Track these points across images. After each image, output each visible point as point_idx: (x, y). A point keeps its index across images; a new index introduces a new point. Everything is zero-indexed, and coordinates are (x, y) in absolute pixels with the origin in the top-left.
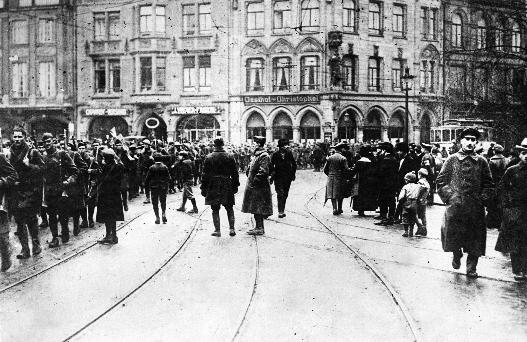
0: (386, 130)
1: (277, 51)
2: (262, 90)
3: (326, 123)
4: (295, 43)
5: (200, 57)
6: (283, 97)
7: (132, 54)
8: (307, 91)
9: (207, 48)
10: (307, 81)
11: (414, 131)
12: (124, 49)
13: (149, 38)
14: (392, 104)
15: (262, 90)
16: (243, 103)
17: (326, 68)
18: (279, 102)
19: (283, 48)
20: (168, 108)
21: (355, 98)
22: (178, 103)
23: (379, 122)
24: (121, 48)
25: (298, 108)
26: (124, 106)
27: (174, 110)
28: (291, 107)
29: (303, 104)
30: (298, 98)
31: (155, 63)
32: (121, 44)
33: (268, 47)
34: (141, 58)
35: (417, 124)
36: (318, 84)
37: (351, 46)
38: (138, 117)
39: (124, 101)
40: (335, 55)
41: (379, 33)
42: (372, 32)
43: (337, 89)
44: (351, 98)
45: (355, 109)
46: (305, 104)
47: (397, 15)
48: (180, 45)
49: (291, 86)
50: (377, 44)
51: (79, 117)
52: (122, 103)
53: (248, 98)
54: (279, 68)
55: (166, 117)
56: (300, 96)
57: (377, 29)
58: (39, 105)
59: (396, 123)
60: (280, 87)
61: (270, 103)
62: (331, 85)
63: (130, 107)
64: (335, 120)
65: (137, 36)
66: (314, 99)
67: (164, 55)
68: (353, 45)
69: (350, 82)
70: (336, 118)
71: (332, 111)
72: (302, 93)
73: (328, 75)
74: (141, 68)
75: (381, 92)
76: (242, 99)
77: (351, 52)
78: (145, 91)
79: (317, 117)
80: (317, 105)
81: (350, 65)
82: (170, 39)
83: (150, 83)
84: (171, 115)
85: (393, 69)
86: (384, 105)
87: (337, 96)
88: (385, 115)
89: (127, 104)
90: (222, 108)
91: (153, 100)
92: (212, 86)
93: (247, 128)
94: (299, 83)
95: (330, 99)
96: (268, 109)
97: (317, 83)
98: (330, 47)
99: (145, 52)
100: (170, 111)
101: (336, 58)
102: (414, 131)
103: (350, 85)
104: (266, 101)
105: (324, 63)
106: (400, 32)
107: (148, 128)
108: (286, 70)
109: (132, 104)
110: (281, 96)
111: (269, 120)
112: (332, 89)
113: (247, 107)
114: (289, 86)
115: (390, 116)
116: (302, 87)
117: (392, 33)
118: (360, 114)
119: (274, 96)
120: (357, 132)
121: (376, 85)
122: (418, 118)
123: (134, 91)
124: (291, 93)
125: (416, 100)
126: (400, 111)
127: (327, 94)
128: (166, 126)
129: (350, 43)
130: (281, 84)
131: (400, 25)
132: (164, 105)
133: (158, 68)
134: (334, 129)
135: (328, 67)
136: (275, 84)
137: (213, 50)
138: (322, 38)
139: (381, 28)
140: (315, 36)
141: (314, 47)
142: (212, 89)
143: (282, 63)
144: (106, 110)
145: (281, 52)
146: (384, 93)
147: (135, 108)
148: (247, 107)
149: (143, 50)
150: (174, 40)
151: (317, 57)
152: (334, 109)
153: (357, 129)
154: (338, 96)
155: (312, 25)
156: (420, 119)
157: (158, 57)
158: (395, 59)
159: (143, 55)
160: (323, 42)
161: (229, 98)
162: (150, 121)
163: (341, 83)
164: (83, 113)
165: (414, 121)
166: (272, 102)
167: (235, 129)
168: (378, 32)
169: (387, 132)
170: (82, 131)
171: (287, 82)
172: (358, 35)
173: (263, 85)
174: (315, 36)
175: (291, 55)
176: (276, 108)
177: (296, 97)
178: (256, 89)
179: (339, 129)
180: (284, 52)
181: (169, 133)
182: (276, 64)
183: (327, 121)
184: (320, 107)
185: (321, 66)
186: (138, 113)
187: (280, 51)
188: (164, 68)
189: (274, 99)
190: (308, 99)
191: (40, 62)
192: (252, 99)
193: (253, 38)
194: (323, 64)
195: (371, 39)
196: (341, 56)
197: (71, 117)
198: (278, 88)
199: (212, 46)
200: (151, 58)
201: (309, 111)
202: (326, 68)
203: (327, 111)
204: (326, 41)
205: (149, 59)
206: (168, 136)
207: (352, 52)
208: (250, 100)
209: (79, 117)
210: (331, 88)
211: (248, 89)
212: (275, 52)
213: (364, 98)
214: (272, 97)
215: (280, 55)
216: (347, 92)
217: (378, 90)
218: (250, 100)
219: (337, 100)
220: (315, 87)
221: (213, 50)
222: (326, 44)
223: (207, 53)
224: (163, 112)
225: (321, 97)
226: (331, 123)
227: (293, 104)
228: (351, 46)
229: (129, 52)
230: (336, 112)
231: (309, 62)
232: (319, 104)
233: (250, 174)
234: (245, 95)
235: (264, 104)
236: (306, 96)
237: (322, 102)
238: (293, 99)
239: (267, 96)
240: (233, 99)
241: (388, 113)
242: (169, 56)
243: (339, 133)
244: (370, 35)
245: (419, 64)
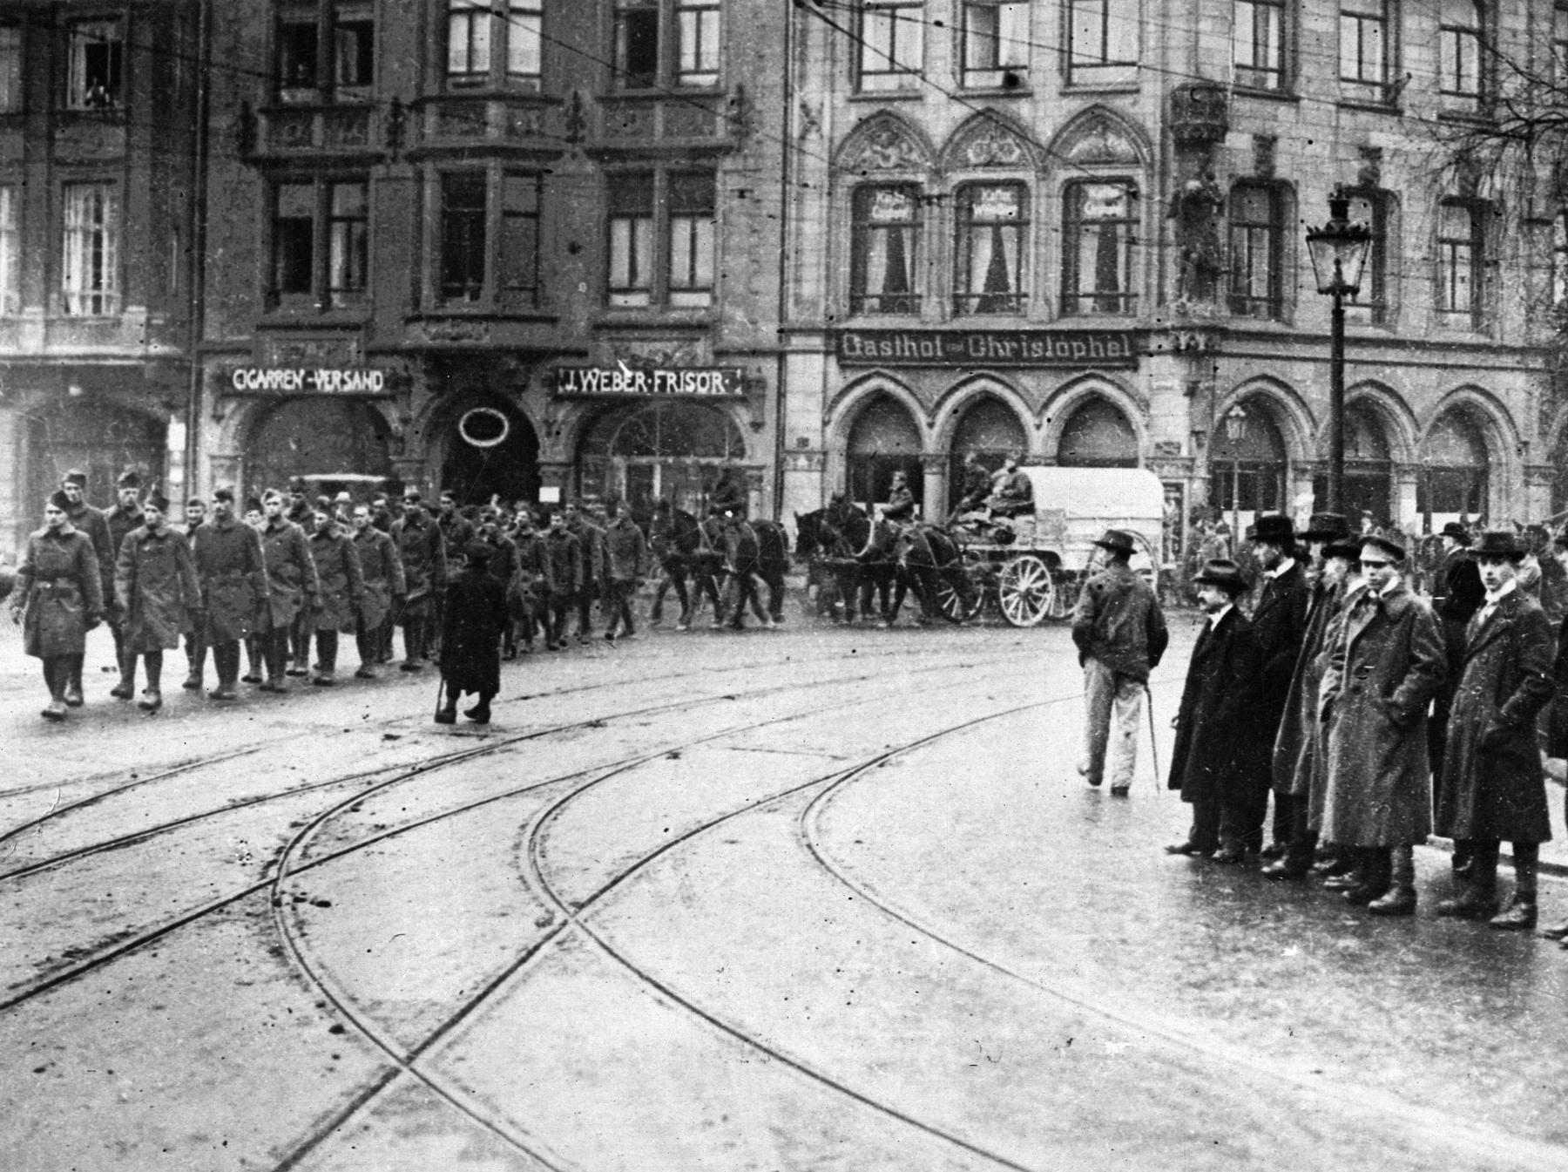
0: (1408, 478)
1: (973, 159)
2: (915, 311)
3: (1158, 446)
4: (1045, 132)
5: (672, 175)
6: (905, 338)
7: (412, 158)
8: (1090, 317)
9: (699, 141)
10: (1088, 281)
11: (1527, 484)
12: (385, 138)
13: (476, 98)
14: (1434, 373)
15: (915, 311)
16: (833, 360)
17: (1162, 229)
18: (975, 359)
19: (995, 146)
20: (544, 370)
21: (1281, 350)
22: (582, 354)
23: (1382, 444)
24: (375, 138)
25: (1050, 383)
26: (380, 360)
27: (566, 380)
28: (1027, 381)
29: (1069, 370)
30: (938, 343)
31: (501, 192)
32: (373, 120)
33: (938, 142)
34: (445, 176)
35: (1538, 456)
36: (1132, 291)
37: (1266, 144)
38: (432, 399)
39: (381, 340)
40: (1198, 177)
41: (1480, 108)
42: (1352, 92)
43: (1202, 310)
44: (1262, 348)
45: (1281, 393)
46: (1075, 369)
47: (1459, 30)
48: (597, 136)
49: (1026, 295)
50: (1270, 128)
51: (207, 397)
52: (372, 345)
53: (857, 339)
54: (982, 224)
55: (535, 406)
56: (1056, 335)
57: (1374, 84)
58: (55, 349)
59: (1455, 453)
60: (984, 298)
61: (943, 359)
62: (1180, 296)
63: (398, 363)
64: (1194, 433)
65: (432, 89)
66: (1113, 349)
67: (531, 164)
68: (1275, 139)
69: (1259, 289)
70: (1198, 428)
71: (1186, 401)
72: (958, 325)
73: (1172, 253)
74: (444, 214)
75: (1289, 324)
76: (834, 342)
77: (1263, 168)
78: (452, 307)
79: (1120, 417)
80: (1127, 374)
81: (1465, 233)
82: (560, 102)
83: (480, 279)
84: (559, 399)
85: (1443, 241)
86: (1406, 381)
87: (1201, 339)
88: (1404, 419)
89: (394, 352)
90: (753, 375)
91: (486, 337)
92: (718, 292)
93: (851, 457)
94: (1055, 289)
95: (1177, 352)
96: (1036, 384)
97: (1127, 288)
98: (1181, 145)
99: (456, 153)
100: (553, 382)
101: (1199, 191)
102: (1527, 484)
103: (1365, 306)
104: (924, 354)
105: (1156, 208)
106: (1470, 96)
107: (477, 449)
108: (1008, 232)
109: (410, 353)
110: (985, 333)
111: (937, 429)
112: (1183, 313)
113: (853, 376)
114: (1020, 295)
115: (1426, 426)
116: (1068, 302)
117: (1436, 99)
118: (1299, 413)
119: (953, 332)
120: (1289, 484)
121: (1368, 301)
122: (1543, 434)
123: (416, 302)
124: (912, 324)
125: (1539, 363)
126: (1468, 403)
127: (1164, 332)
128: (535, 445)
129: (1260, 133)
130: (987, 286)
131: (1472, 67)
132: (532, 357)
133: (508, 214)
134: (1190, 468)
135: (1171, 224)
136: (962, 291)
137: (726, 150)
138: (1148, 109)
139: (1391, 80)
140: (1121, 103)
141: (1120, 145)
142: (714, 299)
143: (996, 205)
144: (310, 374)
145: (988, 164)
146: (1403, 332)
147: (418, 370)
148: (853, 376)
149: (454, 141)
150: (577, 106)
151: (1130, 181)
152: (1191, 392)
153: (1290, 475)
154: (1210, 339)
155: (1113, 55)
156: (1553, 441)
157: (510, 172)
158: (1449, 202)
159: (448, 164)
160: (1153, 126)
161: (780, 339)
162: (479, 416)
163: (1222, 288)
164: (223, 381)
165: (1526, 444)
166: (948, 356)
167: (802, 461)
168: (1378, 91)
169: (1413, 488)
170: (215, 451)
171: (1012, 280)
172: (1297, 100)
173: (917, 291)
174: (1121, 103)
175: (1028, 176)
176: (964, 383)
177: (933, 340)
178: (887, 306)
179: (1214, 467)
180: (1001, 164)
181: (544, 469)
182: (970, 210)
183: (1161, 439)
184: (1139, 381)
185: (1143, 217)
186: (429, 387)
187: (982, 159)
188: (535, 216)
189: (960, 348)
190: (1088, 350)
191: (67, 184)
192: (870, 344)
193: (882, 106)
194: (1150, 215)
195: (1346, 119)
196: (1224, 185)
197: (180, 399)
198: (975, 302)
199: (721, 132)
200: (483, 173)
201: (881, 397)
202: (1162, 229)
203: (1166, 396)
204: (1164, 121)
205: (478, 179)
206: (545, 480)
207: (1272, 168)
208: (863, 349)
209: (207, 397)
210: (1183, 305)
211: (855, 307)
212: (966, 165)
213: (1317, 348)
214: (951, 336)
215: (980, 175)
216: (1254, 325)
217: (1378, 319)
218: (863, 349)
219: (1205, 353)
220: (1122, 300)
221: (726, 150)
222: (1163, 133)
223: (703, 162)
224: (523, 388)
225: (1142, 343)
226: (1179, 448)
227: (1034, 366)
228: (1266, 144)
229: (402, 152)
230: (1203, 405)
231: (1099, 203)
232: (1136, 368)
233: (655, 652)
234: (843, 326)
235: (921, 366)
236: (1081, 335)
237: (1144, 361)
238: (1030, 349)
239: (929, 335)
240: (796, 342)
241: (1417, 410)
242: (558, 167)
243: (1213, 483)
244: (1342, 105)
245: (1548, 223)
